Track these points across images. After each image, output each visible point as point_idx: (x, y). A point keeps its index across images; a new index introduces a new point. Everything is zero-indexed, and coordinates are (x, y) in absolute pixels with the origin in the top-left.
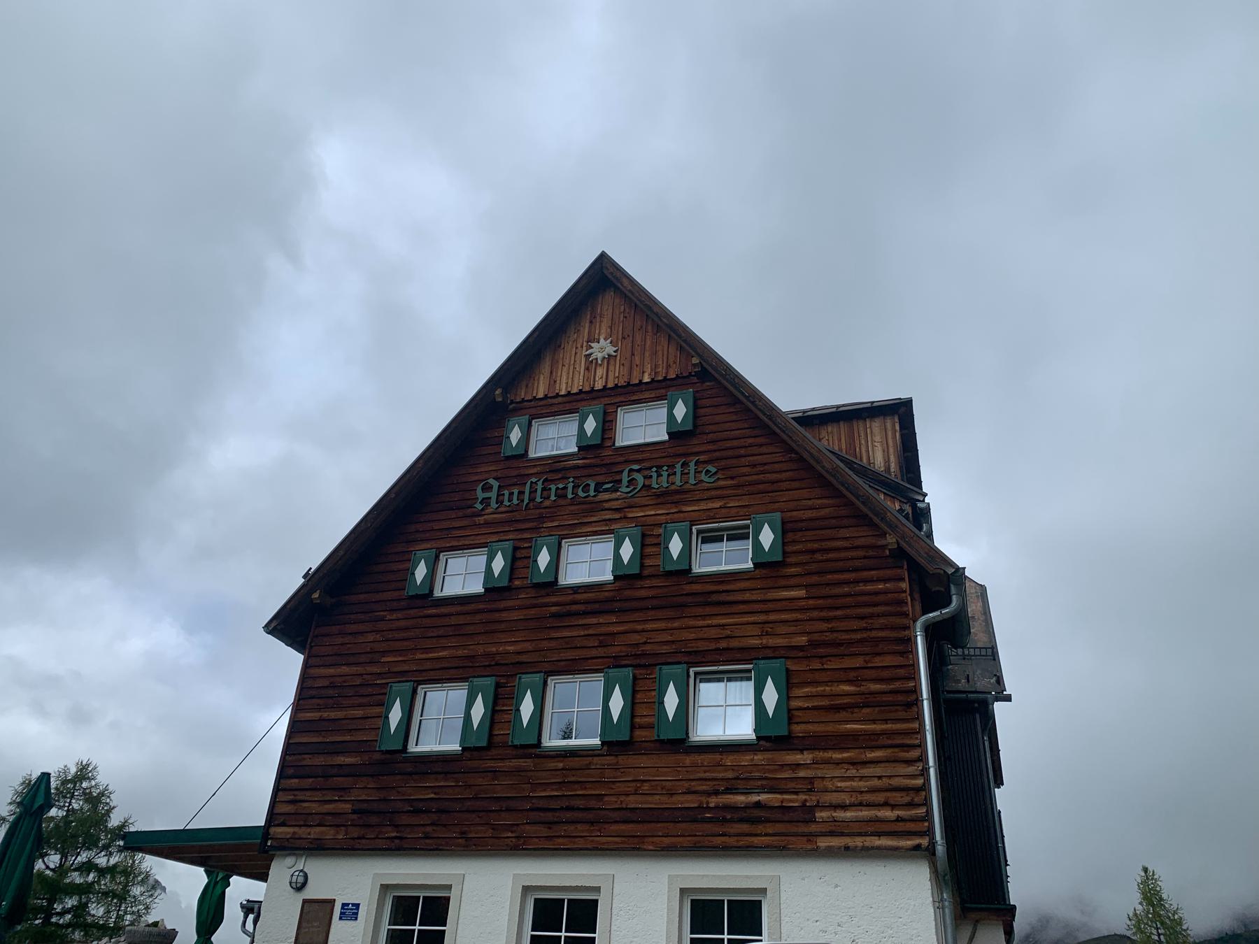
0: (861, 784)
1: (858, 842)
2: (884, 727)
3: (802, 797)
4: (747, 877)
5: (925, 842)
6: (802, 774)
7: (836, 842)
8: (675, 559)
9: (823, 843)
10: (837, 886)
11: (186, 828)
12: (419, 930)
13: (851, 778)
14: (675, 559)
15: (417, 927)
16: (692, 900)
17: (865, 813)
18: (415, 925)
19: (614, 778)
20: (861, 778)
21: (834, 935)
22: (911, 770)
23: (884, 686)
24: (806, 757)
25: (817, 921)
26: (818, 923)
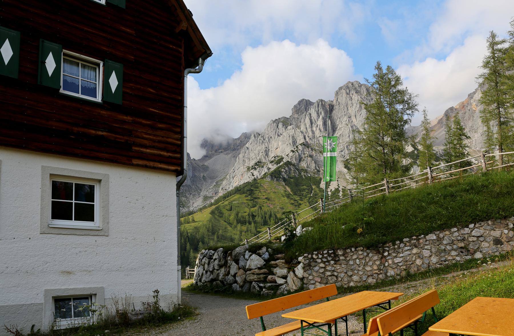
0: (154, 138)
1: (151, 164)
2: (167, 114)
3: (126, 138)
4: (91, 173)
5: (179, 169)
6: (126, 127)
7: (141, 162)
8: (7, 40)
9: (135, 162)
10: (137, 183)
11: (327, 331)
12: (72, 203)
13: (150, 134)
14: (7, 40)
15: (74, 201)
16: (52, 181)
17: (155, 152)
18: (75, 201)
19: (71, 74)
20: (154, 135)
21: (134, 204)
22: (176, 136)
23: (168, 95)
24: (129, 118)
25: (127, 197)
26: (127, 198)
